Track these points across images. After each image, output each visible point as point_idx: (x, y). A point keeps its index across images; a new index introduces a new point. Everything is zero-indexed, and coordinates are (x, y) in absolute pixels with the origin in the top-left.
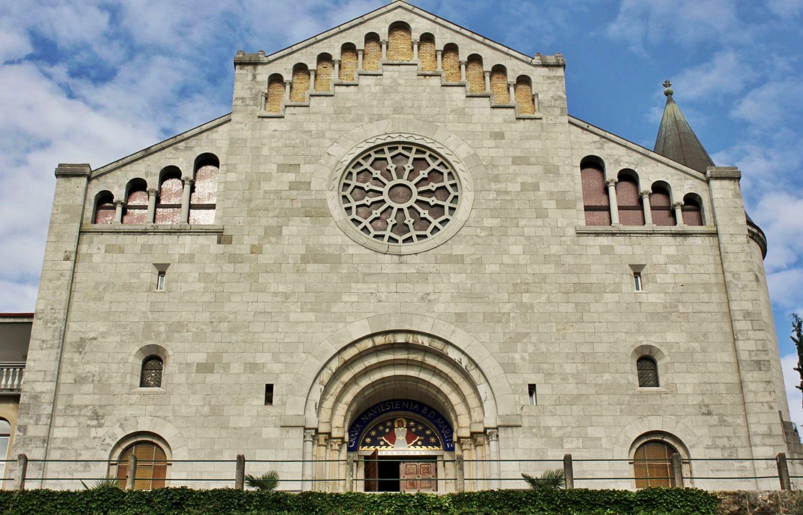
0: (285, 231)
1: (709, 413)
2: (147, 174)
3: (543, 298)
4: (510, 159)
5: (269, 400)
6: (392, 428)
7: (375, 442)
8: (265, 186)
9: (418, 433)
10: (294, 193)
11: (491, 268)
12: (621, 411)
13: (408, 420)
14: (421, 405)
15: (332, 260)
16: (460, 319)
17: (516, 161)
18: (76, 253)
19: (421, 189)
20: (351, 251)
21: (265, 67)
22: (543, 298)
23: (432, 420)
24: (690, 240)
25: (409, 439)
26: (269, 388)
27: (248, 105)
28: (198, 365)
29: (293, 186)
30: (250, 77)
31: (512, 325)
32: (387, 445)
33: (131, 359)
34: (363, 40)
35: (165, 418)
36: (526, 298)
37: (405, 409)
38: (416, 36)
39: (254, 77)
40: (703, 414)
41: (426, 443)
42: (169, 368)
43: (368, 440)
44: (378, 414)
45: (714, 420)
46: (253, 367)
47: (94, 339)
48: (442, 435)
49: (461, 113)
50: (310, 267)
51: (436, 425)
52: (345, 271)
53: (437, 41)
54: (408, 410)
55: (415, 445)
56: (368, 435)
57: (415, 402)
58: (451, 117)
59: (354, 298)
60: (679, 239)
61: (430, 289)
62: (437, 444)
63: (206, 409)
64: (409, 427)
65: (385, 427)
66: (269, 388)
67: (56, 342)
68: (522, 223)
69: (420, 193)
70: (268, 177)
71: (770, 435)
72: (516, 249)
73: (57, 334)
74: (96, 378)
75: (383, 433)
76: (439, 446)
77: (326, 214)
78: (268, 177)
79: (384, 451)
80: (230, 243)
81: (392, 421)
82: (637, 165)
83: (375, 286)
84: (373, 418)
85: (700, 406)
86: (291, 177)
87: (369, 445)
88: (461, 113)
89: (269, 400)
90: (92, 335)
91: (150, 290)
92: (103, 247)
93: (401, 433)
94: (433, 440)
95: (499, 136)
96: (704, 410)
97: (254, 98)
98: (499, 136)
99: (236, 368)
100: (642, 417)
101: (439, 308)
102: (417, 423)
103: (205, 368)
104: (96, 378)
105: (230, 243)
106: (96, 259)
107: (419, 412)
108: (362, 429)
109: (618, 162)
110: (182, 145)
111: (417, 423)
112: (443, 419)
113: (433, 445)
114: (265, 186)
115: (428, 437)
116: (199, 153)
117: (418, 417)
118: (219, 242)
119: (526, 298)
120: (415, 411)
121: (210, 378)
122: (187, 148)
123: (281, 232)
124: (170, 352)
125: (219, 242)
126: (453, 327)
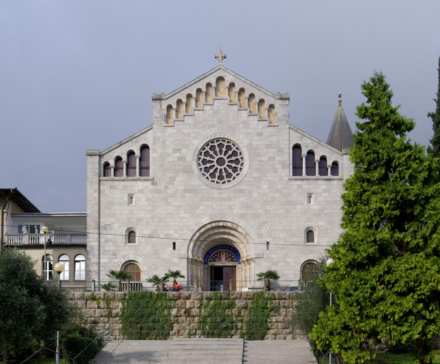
2: (122, 154)
5: (174, 248)
6: (220, 255)
7: (214, 261)
8: (169, 159)
9: (229, 257)
10: (179, 162)
11: (255, 195)
13: (226, 252)
16: (243, 216)
17: (267, 146)
19: (229, 159)
20: (202, 187)
21: (165, 101)
22: (274, 207)
24: (332, 182)
25: (226, 260)
27: (159, 121)
29: (179, 159)
30: (159, 107)
32: (218, 262)
35: (138, 255)
36: (267, 207)
38: (227, 84)
41: (232, 261)
43: (212, 260)
47: (110, 225)
49: (245, 124)
50: (187, 195)
52: (200, 196)
55: (228, 262)
56: (212, 258)
57: (228, 246)
58: (241, 125)
59: (204, 208)
60: (328, 182)
64: (226, 255)
65: (218, 255)
67: (96, 226)
68: (268, 175)
70: (169, 155)
72: (265, 187)
73: (96, 223)
75: (217, 257)
77: (192, 172)
78: (169, 155)
79: (218, 264)
81: (220, 252)
82: (315, 148)
83: (211, 202)
84: (213, 252)
86: (178, 155)
87: (212, 262)
88: (245, 124)
89: (174, 248)
90: (109, 223)
92: (108, 187)
93: (223, 257)
95: (260, 134)
98: (260, 134)
101: (235, 211)
102: (229, 253)
106: (107, 192)
107: (229, 249)
111: (229, 253)
113: (235, 262)
115: (233, 258)
116: (141, 144)
117: (232, 253)
118: (152, 184)
119: (267, 207)
120: (228, 249)
122: (137, 142)
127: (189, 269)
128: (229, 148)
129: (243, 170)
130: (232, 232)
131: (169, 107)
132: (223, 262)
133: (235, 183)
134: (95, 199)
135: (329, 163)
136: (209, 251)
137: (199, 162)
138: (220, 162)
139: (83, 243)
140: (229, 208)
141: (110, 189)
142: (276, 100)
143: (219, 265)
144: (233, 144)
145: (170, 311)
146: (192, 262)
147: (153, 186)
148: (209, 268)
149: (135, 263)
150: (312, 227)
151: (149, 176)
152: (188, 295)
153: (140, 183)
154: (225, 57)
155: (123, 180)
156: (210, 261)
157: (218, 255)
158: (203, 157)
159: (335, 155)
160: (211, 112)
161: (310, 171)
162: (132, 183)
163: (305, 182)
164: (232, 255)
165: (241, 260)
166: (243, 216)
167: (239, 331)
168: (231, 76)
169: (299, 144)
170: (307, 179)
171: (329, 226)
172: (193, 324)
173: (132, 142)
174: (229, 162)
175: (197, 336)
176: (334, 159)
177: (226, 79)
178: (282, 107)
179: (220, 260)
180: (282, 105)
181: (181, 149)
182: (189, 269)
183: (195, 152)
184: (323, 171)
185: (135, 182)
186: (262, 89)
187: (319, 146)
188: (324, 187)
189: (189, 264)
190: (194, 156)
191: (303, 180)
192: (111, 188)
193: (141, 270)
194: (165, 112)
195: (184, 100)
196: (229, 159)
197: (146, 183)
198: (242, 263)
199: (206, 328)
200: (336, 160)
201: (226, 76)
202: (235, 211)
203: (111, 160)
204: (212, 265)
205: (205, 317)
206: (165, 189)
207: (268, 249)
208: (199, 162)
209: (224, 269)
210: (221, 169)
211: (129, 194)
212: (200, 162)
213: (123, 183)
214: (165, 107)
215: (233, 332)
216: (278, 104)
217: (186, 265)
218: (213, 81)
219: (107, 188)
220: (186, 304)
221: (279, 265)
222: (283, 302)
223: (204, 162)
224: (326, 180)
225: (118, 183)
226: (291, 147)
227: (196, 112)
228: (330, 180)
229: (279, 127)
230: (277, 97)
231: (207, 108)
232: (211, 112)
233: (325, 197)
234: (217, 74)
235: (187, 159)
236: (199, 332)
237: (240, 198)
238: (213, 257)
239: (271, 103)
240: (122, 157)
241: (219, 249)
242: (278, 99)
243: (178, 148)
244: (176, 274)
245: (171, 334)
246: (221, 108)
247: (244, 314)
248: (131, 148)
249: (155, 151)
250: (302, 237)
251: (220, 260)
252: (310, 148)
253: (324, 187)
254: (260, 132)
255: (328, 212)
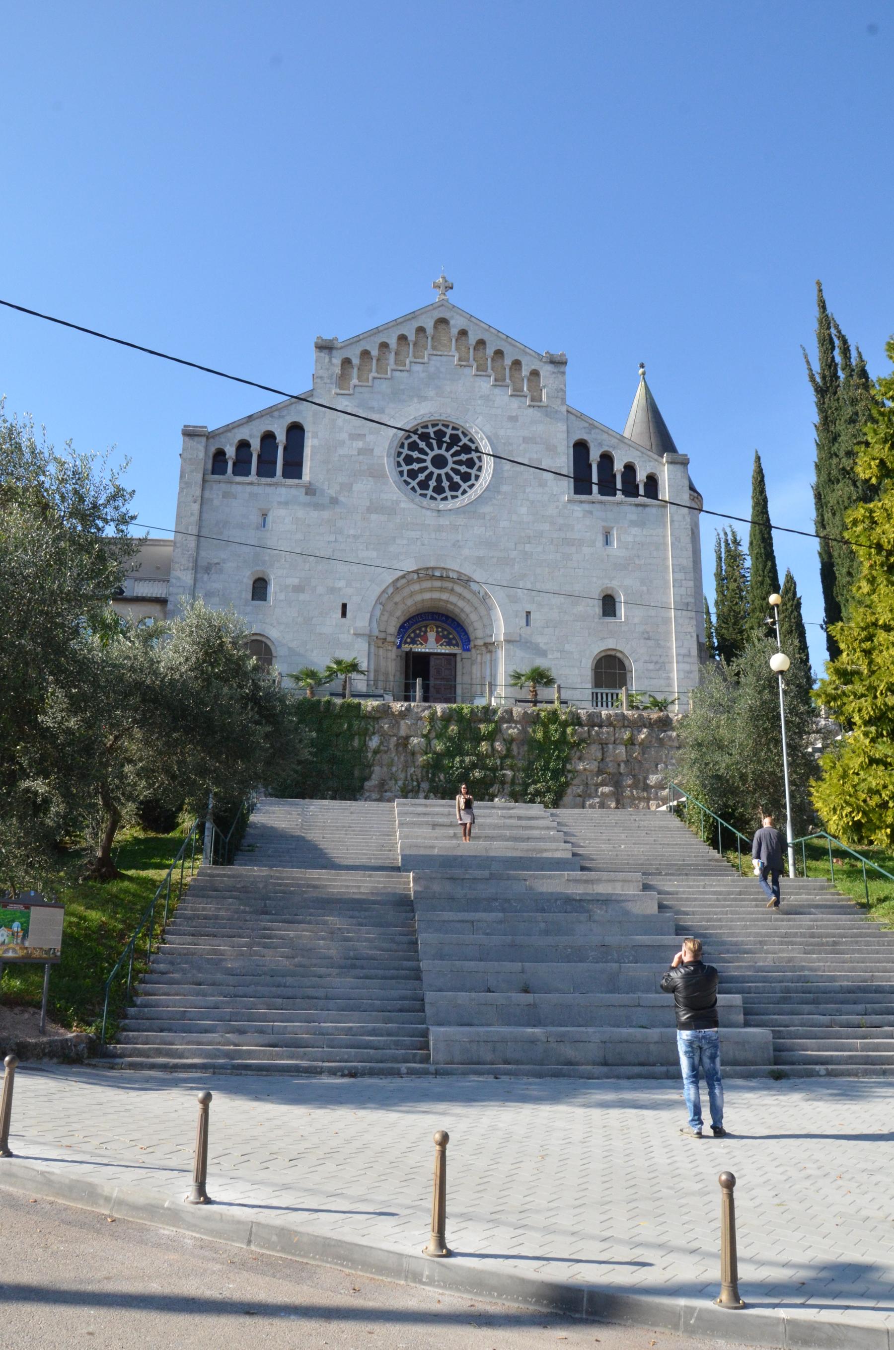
0: (356, 487)
1: (648, 638)
2: (251, 436)
3: (540, 549)
4: (521, 439)
5: (344, 614)
6: (426, 632)
7: (414, 642)
8: (341, 451)
9: (444, 637)
10: (361, 457)
11: (503, 524)
12: (589, 634)
13: (437, 627)
14: (447, 617)
15: (390, 511)
16: (480, 561)
17: (526, 440)
18: (202, 497)
19: (456, 459)
20: (403, 505)
21: (339, 351)
22: (540, 549)
23: (455, 629)
24: (648, 509)
25: (437, 641)
26: (344, 606)
27: (325, 383)
28: (294, 586)
29: (360, 452)
30: (327, 360)
31: (517, 566)
32: (422, 644)
33: (245, 580)
34: (414, 331)
35: (271, 625)
36: (528, 547)
37: (436, 620)
38: (454, 331)
39: (330, 361)
40: (645, 638)
41: (449, 644)
42: (272, 589)
43: (409, 640)
44: (416, 622)
45: (651, 643)
46: (332, 590)
47: (218, 564)
48: (461, 639)
49: (487, 399)
50: (374, 517)
51: (458, 632)
52: (398, 521)
53: (524, 367)
54: (438, 620)
55: (441, 645)
56: (409, 637)
57: (443, 615)
58: (479, 402)
59: (405, 542)
60: (640, 508)
61: (460, 537)
62: (457, 645)
63: (300, 619)
64: (437, 632)
65: (421, 631)
66: (344, 606)
67: (191, 565)
68: (528, 490)
69: (454, 463)
70: (342, 443)
71: (689, 655)
72: (523, 510)
73: (191, 559)
74: (221, 593)
75: (418, 636)
76: (458, 646)
77: (383, 476)
78: (342, 443)
79: (419, 649)
80: (314, 494)
81: (426, 627)
82: (614, 448)
83: (419, 533)
84: (413, 625)
85: (643, 633)
86: (360, 444)
87: (409, 644)
88: (487, 399)
89: (344, 614)
90: (216, 561)
91: (257, 529)
92: (220, 493)
93: (432, 636)
94: (454, 642)
95: (513, 419)
96: (646, 636)
97: (330, 377)
98: (513, 419)
99: (320, 590)
100: (603, 639)
101: (466, 552)
102: (444, 629)
103: (298, 589)
104: (221, 593)
105: (314, 494)
106: (216, 502)
107: (445, 622)
108: (405, 632)
109: (600, 445)
110: (276, 414)
111: (444, 629)
112: (462, 628)
113: (454, 645)
114: (341, 451)
115: (450, 640)
116: (290, 421)
117: (445, 626)
118: (306, 494)
119: (528, 547)
120: (443, 621)
121: (302, 597)
122: (281, 417)
123: (351, 487)
124: (272, 577)
125: (306, 494)
126: (475, 567)
127: (372, 655)
128: (455, 439)
129: (481, 479)
130: (458, 589)
131: (347, 362)
132: (431, 645)
133: (466, 502)
134: (192, 514)
135: (641, 476)
136: (405, 623)
137: (399, 459)
138: (439, 462)
139: (159, 596)
140: (454, 545)
141: (223, 497)
142: (542, 364)
143: (423, 650)
144: (463, 433)
145: (365, 741)
146: (376, 641)
147: (308, 497)
148: (404, 655)
149: (264, 639)
150: (612, 589)
151: (300, 478)
152: (403, 709)
153: (283, 490)
154: (451, 288)
155: (251, 484)
156: (406, 643)
157: (421, 631)
158: (405, 451)
159: (652, 464)
160: (423, 375)
161: (607, 488)
162: (269, 490)
163: (597, 506)
164: (450, 633)
165: (472, 644)
166: (480, 561)
167: (507, 789)
168: (462, 319)
169: (586, 441)
170: (601, 502)
171: (645, 588)
172: (413, 769)
173: (272, 417)
174: (454, 463)
175: (422, 795)
176: (626, 460)
177: (452, 322)
178: (554, 376)
179: (426, 640)
180: (554, 373)
181: (365, 435)
182: (372, 655)
183: (392, 442)
184: (631, 489)
185: (273, 488)
186: (518, 344)
187: (622, 445)
188: (634, 517)
189: (372, 647)
190: (389, 448)
191: (593, 502)
192: (226, 495)
193: (274, 654)
194: (338, 370)
195: (375, 353)
196: (456, 459)
197: (294, 491)
198: (473, 651)
199: (439, 777)
200: (653, 471)
201: (452, 317)
202: (466, 552)
203: (228, 446)
204: (408, 650)
205: (439, 756)
206: (331, 503)
207: (528, 624)
208: (399, 459)
209: (432, 659)
210: (439, 475)
211: (260, 509)
212: (401, 459)
213: (249, 488)
214: (337, 361)
215: (494, 789)
216: (545, 371)
217: (367, 648)
218: (429, 325)
219: (217, 495)
220: (399, 728)
221: (550, 656)
222: (596, 732)
223: (409, 460)
224: (637, 505)
225: (239, 487)
226: (571, 445)
227: (398, 374)
228: (644, 506)
229: (549, 409)
230: (544, 360)
231: (417, 368)
232: (423, 375)
233: (635, 536)
234: (437, 314)
235: (377, 452)
236: (425, 785)
237: (476, 528)
238: (412, 635)
239: (533, 367)
240: (252, 442)
241: (426, 620)
242: (545, 362)
243: (360, 432)
244: (353, 667)
245: (366, 787)
246: (443, 370)
247: (519, 753)
248: (270, 428)
249: (315, 435)
250: (597, 608)
251: (426, 640)
252: (605, 448)
253: (634, 517)
254: (514, 414)
255: (642, 562)
